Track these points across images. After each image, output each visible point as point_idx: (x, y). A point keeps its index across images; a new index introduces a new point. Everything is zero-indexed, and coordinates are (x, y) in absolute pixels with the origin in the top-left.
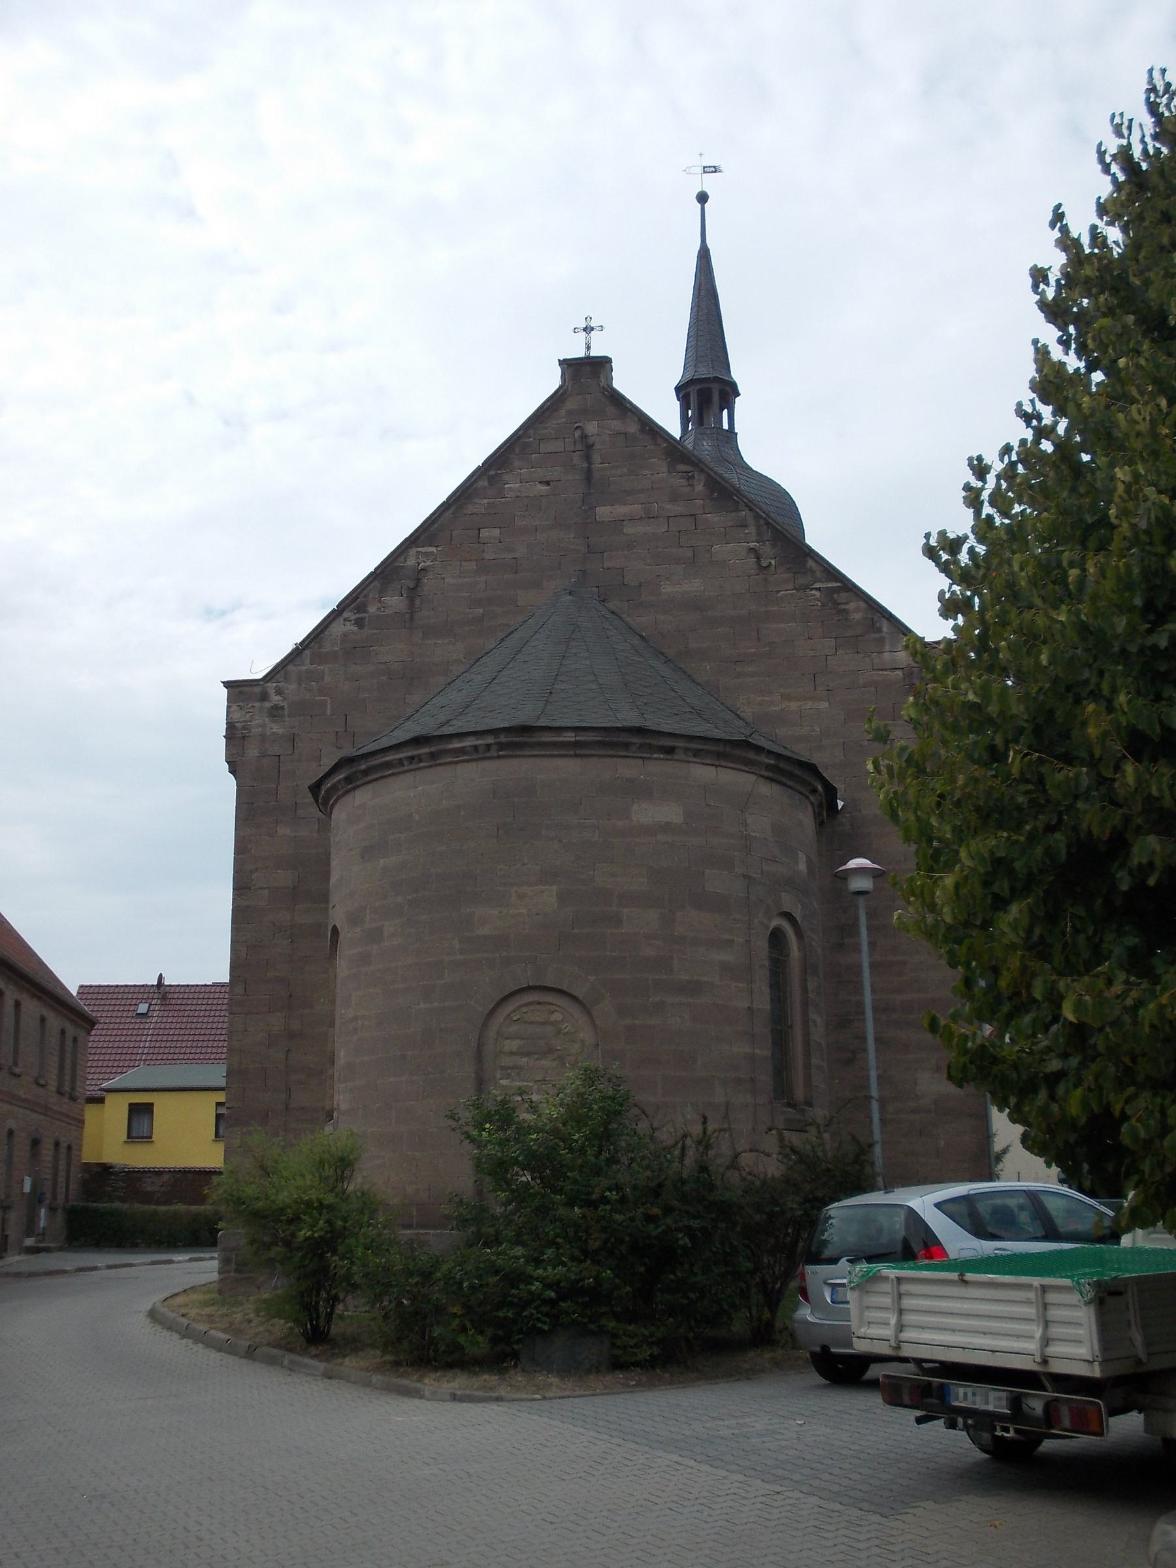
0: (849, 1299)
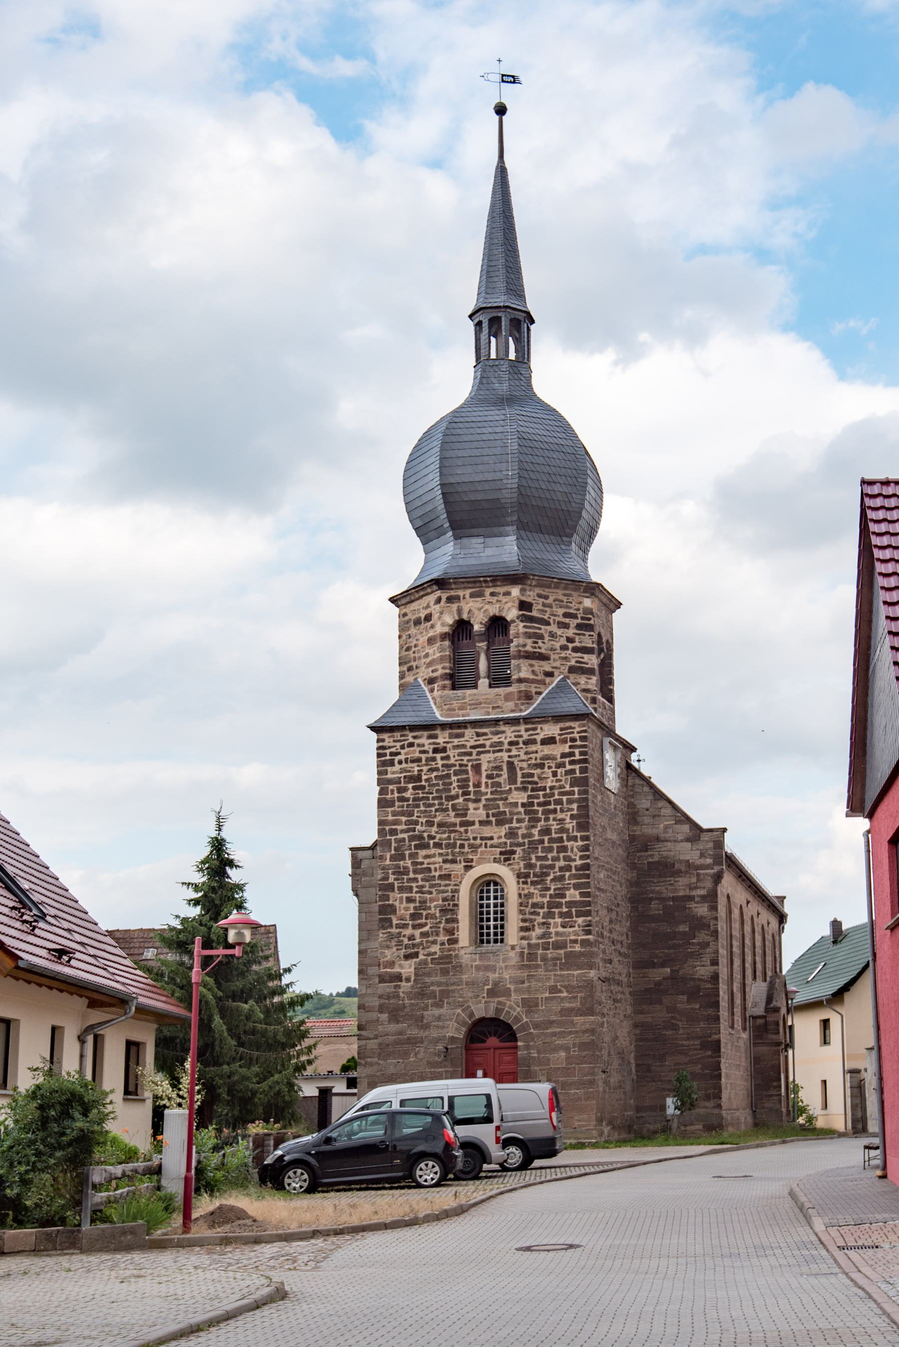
0: (892, 667)
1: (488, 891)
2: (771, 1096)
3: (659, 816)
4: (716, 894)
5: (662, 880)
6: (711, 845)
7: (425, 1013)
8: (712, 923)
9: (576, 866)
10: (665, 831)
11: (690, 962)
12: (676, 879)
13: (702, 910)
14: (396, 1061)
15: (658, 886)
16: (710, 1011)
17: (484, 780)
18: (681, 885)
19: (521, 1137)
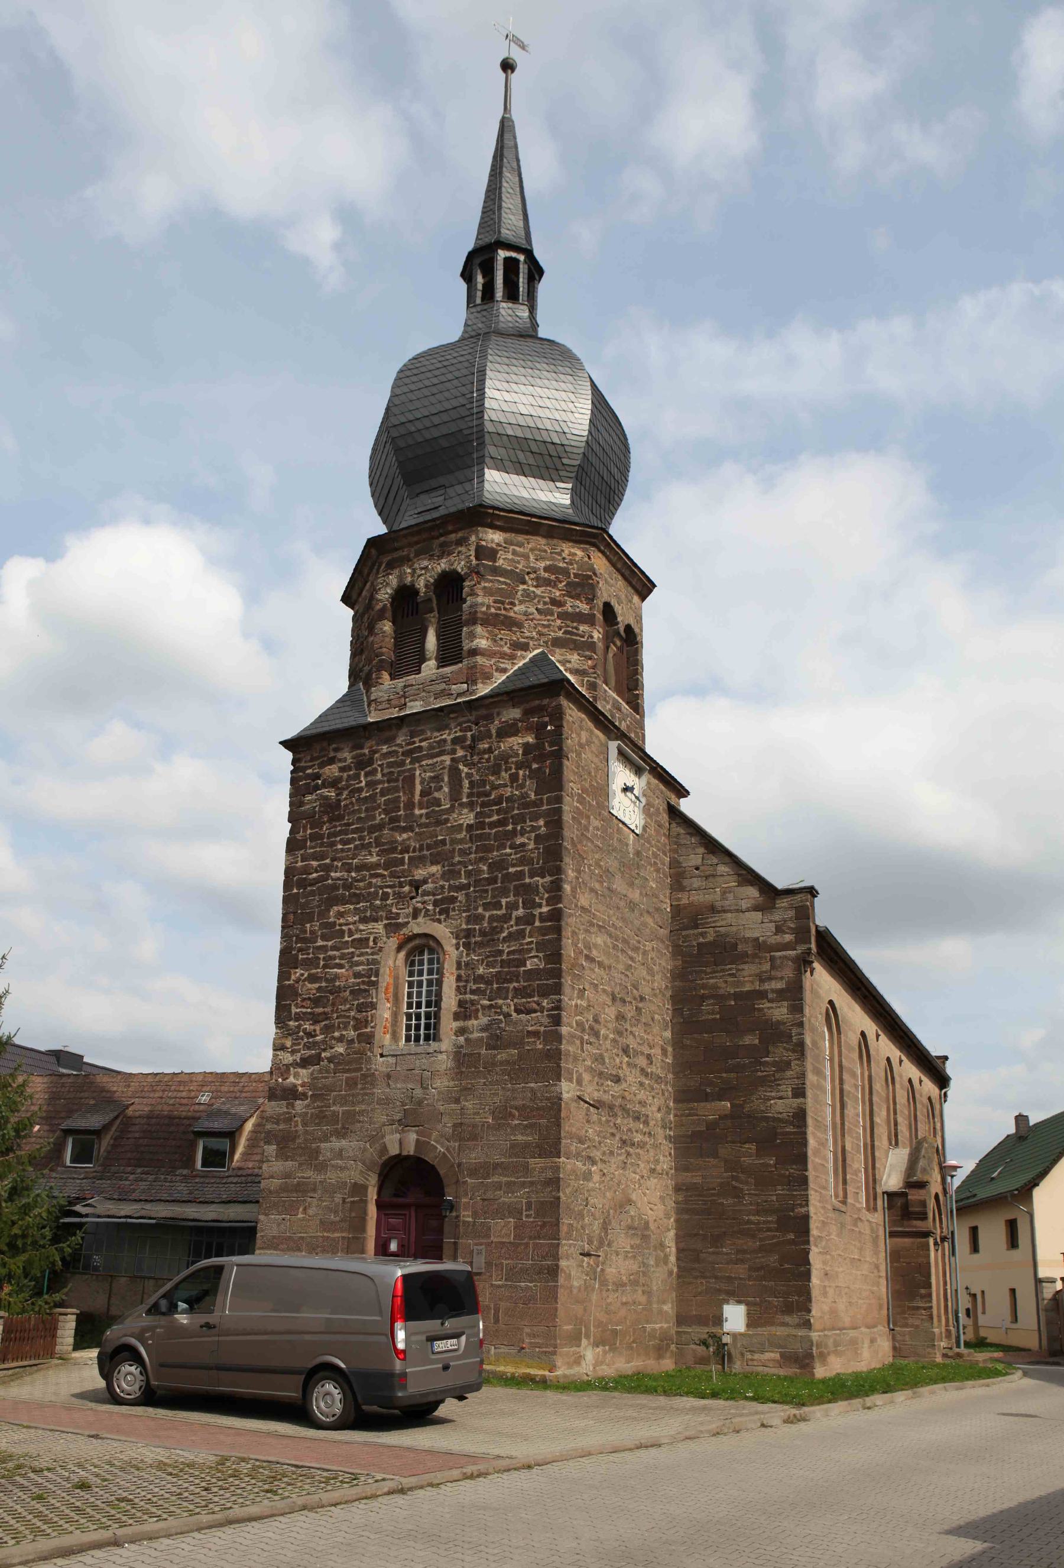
1: (421, 963)
2: (918, 1308)
3: (714, 876)
4: (801, 987)
5: (719, 968)
6: (791, 913)
7: (323, 1145)
8: (794, 1031)
9: (540, 913)
10: (723, 896)
11: (762, 1092)
12: (740, 967)
13: (780, 1012)
14: (281, 1217)
15: (712, 978)
16: (792, 1170)
17: (417, 797)
18: (747, 976)
19: (343, 1365)
